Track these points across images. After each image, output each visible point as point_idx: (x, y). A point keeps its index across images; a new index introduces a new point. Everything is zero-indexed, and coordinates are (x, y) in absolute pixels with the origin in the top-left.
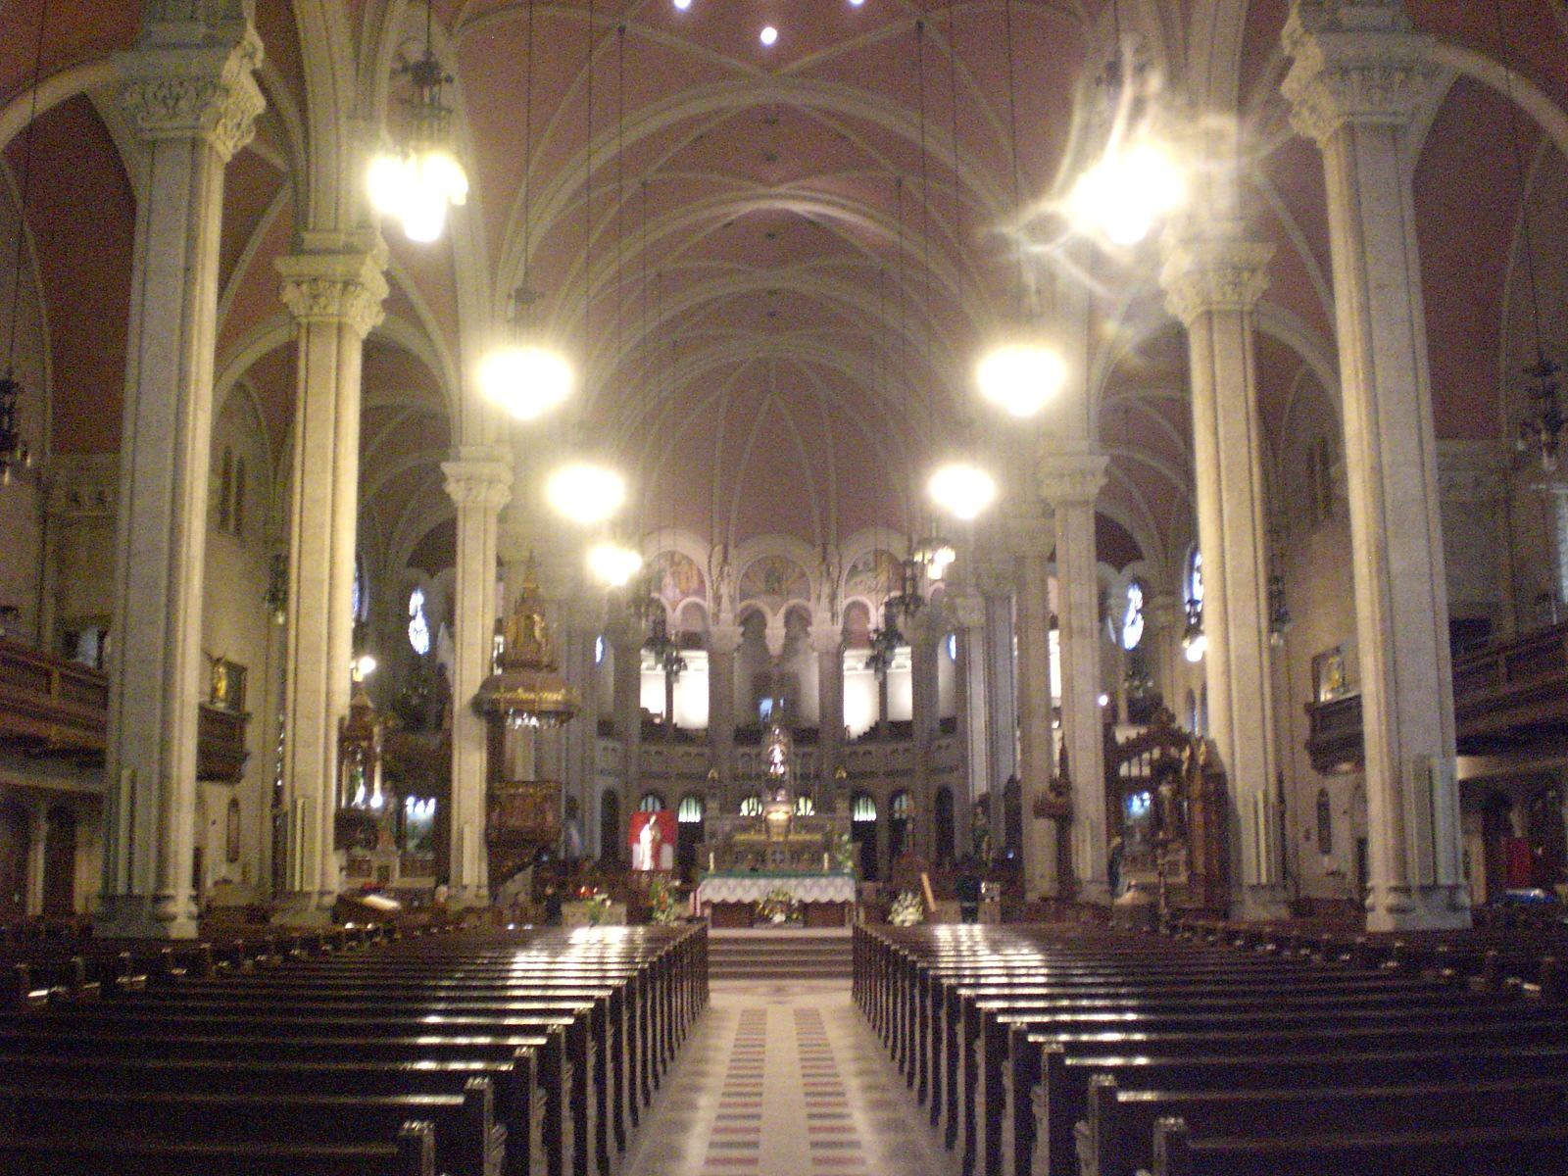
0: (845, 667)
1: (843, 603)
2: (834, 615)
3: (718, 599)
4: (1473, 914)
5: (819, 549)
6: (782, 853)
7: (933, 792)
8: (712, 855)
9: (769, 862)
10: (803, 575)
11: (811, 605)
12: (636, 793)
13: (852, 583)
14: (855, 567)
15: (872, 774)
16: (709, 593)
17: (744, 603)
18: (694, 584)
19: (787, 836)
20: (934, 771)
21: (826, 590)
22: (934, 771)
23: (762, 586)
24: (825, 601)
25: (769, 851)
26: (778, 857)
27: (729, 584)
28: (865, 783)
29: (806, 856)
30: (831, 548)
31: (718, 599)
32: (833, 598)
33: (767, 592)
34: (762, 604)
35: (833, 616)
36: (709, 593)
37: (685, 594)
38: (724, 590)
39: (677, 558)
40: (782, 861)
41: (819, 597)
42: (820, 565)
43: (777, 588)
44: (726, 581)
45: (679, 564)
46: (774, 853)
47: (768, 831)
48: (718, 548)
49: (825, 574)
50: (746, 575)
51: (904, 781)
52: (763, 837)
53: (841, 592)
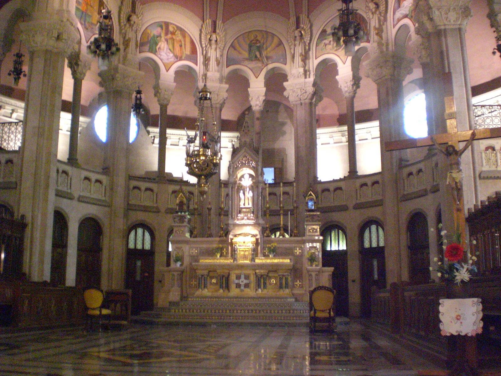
0: (319, 142)
1: (314, 63)
2: (306, 73)
3: (206, 60)
4: (280, 185)
5: (293, 19)
6: (247, 277)
7: (404, 219)
8: (289, 212)
9: (233, 286)
10: (280, 43)
11: (287, 68)
12: (121, 224)
13: (322, 45)
14: (324, 31)
15: (344, 208)
16: (200, 59)
17: (232, 68)
18: (188, 51)
19: (253, 259)
20: (406, 198)
21: (299, 50)
22: (406, 198)
23: (246, 55)
24: (298, 59)
25: (233, 277)
26: (243, 281)
27: (216, 49)
28: (337, 217)
29: (273, 281)
30: (303, 17)
31: (206, 60)
32: (305, 58)
33: (250, 59)
34: (246, 69)
35: (305, 71)
36: (200, 59)
37: (178, 58)
38: (213, 54)
39: (171, 29)
40: (247, 286)
41: (293, 57)
42: (294, 31)
43: (258, 56)
44: (214, 46)
45: (173, 33)
46: (238, 277)
47: (234, 258)
48: (209, 21)
49: (298, 38)
50: (232, 46)
51: (375, 212)
52: (229, 261)
53: (312, 54)
